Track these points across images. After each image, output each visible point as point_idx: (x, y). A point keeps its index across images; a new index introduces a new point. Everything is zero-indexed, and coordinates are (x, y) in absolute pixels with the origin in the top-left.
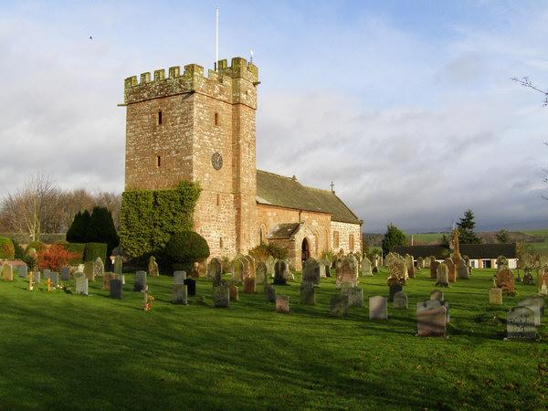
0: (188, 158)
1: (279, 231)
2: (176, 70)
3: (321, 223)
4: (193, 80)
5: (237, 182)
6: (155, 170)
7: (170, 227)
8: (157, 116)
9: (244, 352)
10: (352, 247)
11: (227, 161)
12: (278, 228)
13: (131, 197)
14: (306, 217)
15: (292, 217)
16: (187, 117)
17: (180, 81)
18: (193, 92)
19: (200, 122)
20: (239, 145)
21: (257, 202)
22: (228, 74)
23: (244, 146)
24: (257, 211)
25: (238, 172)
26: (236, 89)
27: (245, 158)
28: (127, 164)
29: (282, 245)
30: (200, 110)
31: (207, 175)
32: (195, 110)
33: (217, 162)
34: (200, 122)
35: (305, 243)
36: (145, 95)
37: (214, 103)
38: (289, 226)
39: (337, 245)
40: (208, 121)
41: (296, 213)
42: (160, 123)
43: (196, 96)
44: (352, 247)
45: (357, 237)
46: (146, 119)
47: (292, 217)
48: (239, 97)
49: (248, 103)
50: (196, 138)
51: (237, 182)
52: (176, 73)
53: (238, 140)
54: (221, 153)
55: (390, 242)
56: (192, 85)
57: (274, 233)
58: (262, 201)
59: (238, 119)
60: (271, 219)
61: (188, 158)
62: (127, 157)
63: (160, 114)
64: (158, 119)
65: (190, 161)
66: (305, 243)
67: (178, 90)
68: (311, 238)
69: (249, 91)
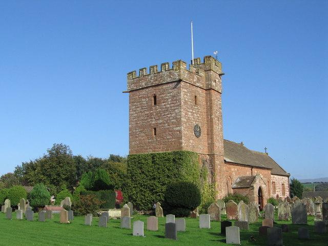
0: (178, 128)
1: (240, 182)
2: (167, 65)
3: (265, 176)
4: (180, 72)
5: (211, 146)
6: (152, 138)
7: (158, 194)
8: (153, 99)
9: (133, 176)
10: (284, 194)
11: (204, 131)
12: (239, 180)
13: (134, 160)
14: (256, 172)
15: (247, 172)
16: (176, 99)
17: (170, 73)
18: (180, 81)
19: (186, 102)
20: (211, 119)
21: (225, 161)
22: (201, 68)
23: (215, 120)
24: (225, 167)
25: (212, 138)
26: (208, 79)
27: (217, 128)
28: (131, 135)
29: (244, 193)
30: (185, 93)
31: (191, 141)
32: (182, 94)
33: (197, 132)
34: (186, 102)
35: (260, 190)
36: (143, 84)
37: (194, 89)
38: (247, 178)
39: (274, 192)
40: (191, 102)
41: (249, 169)
42: (155, 134)
43: (182, 83)
44: (284, 194)
45: (286, 185)
46: (144, 101)
47: (247, 172)
48: (211, 84)
49: (216, 89)
50: (183, 114)
51: (211, 146)
52: (167, 67)
53: (211, 115)
54: (200, 125)
55: (296, 188)
56: (179, 75)
57: (236, 183)
58: (228, 160)
59: (211, 100)
60: (234, 173)
61: (178, 128)
62: (130, 129)
63: (155, 97)
64: (153, 102)
65: (180, 131)
66: (260, 190)
67: (169, 80)
68: (263, 186)
69: (217, 80)
